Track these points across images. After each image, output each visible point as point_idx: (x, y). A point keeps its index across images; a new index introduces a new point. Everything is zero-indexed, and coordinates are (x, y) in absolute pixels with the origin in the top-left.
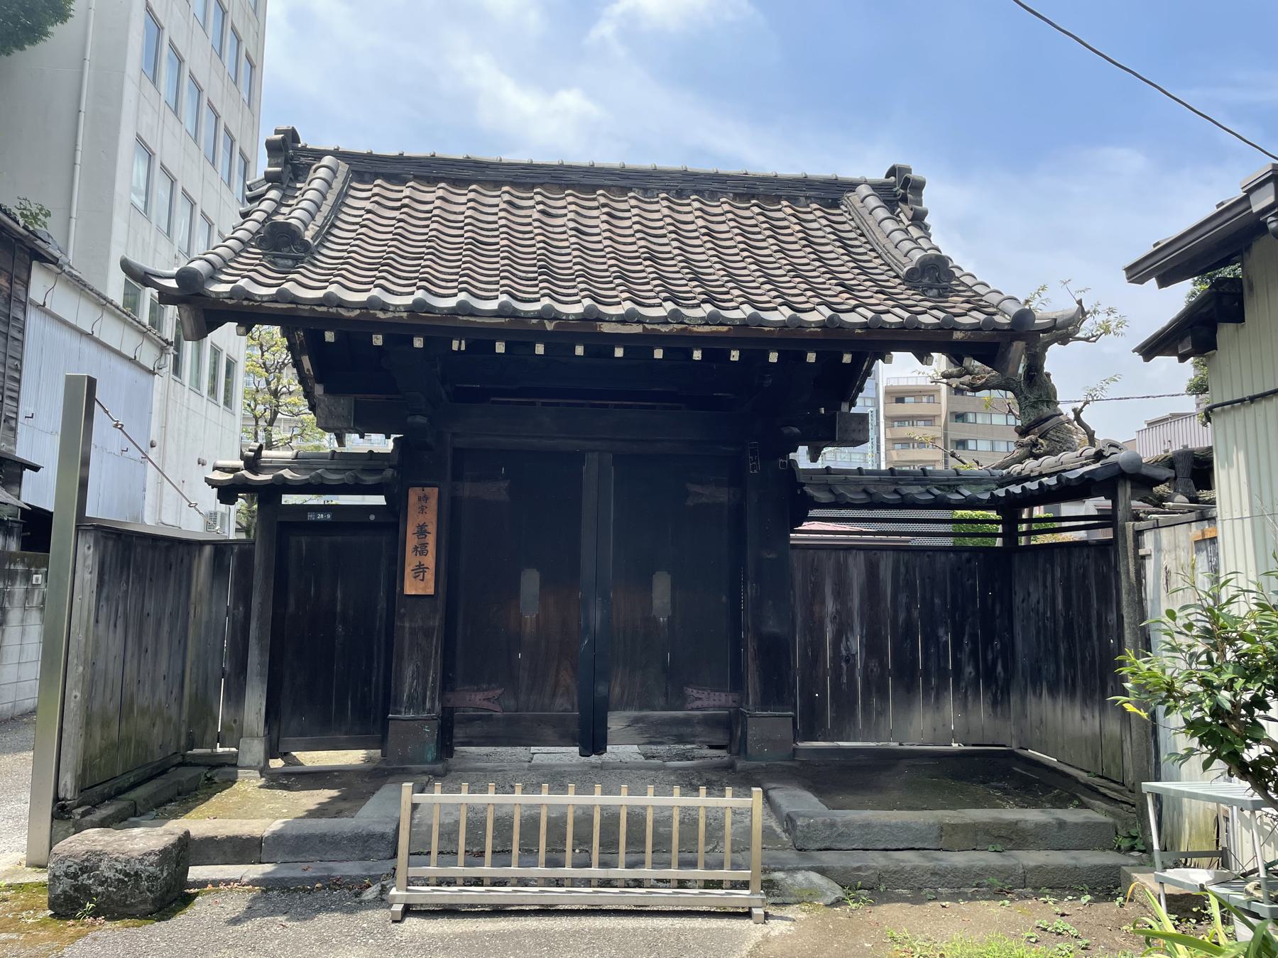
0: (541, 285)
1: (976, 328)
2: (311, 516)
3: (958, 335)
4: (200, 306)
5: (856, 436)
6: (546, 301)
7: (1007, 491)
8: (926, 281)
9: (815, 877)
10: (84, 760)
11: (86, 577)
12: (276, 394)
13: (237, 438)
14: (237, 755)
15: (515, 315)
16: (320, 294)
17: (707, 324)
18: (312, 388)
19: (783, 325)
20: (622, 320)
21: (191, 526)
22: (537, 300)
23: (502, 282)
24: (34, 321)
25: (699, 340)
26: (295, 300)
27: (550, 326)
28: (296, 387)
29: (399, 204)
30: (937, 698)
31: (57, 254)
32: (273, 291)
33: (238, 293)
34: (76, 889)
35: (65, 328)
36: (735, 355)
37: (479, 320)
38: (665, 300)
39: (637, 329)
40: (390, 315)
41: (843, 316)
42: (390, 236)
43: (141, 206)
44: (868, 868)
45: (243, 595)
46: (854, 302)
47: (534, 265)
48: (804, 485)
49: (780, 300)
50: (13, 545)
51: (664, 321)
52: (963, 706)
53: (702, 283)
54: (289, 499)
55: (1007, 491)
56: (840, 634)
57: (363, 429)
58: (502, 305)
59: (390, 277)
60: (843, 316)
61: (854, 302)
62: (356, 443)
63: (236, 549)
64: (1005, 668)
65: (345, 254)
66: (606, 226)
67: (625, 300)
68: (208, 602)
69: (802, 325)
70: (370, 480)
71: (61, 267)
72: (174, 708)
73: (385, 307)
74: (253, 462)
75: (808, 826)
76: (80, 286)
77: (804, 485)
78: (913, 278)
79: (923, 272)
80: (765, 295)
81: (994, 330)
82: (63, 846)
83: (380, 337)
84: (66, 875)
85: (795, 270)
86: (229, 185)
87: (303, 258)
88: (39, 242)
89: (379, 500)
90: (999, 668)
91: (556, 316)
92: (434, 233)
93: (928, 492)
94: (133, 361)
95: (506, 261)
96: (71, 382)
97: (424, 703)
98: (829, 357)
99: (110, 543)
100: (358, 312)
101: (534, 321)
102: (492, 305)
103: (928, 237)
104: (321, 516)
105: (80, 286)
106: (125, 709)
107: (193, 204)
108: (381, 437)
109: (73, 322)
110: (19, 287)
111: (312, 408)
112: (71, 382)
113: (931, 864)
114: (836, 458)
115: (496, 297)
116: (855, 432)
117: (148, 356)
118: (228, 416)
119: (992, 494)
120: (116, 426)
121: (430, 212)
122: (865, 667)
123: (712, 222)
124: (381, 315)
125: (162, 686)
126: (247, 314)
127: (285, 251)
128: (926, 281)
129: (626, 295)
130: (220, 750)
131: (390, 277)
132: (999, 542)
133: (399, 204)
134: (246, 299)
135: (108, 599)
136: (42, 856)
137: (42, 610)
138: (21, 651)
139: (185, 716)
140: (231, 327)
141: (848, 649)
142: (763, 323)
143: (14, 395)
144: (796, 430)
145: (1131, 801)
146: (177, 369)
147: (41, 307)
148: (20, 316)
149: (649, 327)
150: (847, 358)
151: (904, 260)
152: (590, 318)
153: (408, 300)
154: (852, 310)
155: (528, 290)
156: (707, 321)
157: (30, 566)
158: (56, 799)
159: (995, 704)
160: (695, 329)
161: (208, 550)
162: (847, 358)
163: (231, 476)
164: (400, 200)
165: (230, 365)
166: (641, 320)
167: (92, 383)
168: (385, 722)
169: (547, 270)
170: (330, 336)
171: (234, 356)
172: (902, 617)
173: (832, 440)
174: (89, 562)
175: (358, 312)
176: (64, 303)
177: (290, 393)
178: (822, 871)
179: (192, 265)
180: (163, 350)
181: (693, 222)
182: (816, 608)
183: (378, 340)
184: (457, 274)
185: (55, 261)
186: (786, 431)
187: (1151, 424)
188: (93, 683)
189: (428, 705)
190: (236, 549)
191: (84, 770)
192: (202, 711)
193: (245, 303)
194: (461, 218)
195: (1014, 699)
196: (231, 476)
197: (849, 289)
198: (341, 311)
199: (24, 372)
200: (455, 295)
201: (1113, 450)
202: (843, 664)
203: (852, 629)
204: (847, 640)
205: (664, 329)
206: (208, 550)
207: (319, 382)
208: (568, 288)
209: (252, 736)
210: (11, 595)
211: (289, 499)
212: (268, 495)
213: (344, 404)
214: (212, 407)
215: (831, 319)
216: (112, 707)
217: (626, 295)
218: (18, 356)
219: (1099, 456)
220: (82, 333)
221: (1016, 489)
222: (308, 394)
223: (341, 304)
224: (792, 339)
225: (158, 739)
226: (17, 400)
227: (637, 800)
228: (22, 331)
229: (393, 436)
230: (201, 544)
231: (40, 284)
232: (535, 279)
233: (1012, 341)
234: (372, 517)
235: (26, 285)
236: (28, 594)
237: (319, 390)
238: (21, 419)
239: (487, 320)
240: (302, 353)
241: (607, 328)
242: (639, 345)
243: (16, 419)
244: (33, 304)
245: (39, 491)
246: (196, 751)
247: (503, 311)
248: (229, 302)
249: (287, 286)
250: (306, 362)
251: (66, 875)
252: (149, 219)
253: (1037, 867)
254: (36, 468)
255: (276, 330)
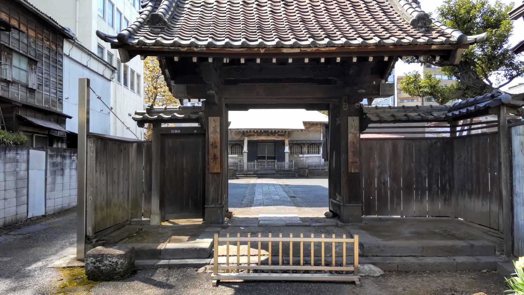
0: (258, 34)
1: (442, 43)
2: (172, 132)
3: (434, 47)
4: (127, 47)
5: (389, 93)
6: (260, 40)
7: (453, 114)
8: (420, 25)
9: (371, 266)
10: (95, 222)
11: (92, 155)
12: (156, 88)
13: (142, 106)
14: (149, 221)
15: (249, 47)
16: (171, 42)
17: (327, 47)
18: (170, 82)
19: (359, 45)
20: (292, 47)
21: (128, 136)
22: (257, 40)
23: (242, 34)
24: (66, 61)
25: (323, 54)
26: (162, 45)
27: (262, 51)
28: (164, 83)
29: (200, 5)
30: (421, 198)
31: (73, 35)
32: (154, 41)
33: (140, 42)
34: (95, 267)
35: (77, 64)
36: (338, 60)
37: (234, 50)
38: (309, 37)
39: (298, 50)
40: (199, 49)
41: (385, 41)
42: (197, 18)
43: (102, 15)
44: (393, 263)
45: (149, 161)
46: (389, 35)
47: (255, 27)
48: (366, 114)
49: (357, 35)
50: (65, 146)
51: (309, 46)
52: (432, 199)
53: (324, 30)
54: (164, 125)
55: (453, 114)
56: (381, 174)
57: (190, 97)
58: (243, 43)
59: (198, 34)
60: (385, 41)
61: (389, 35)
62: (188, 104)
63: (145, 144)
64: (450, 186)
65: (180, 26)
66: (283, 9)
67: (292, 38)
68: (137, 166)
69: (367, 45)
70: (194, 116)
71: (74, 40)
72: (126, 203)
73: (197, 46)
74: (150, 110)
75: (369, 247)
76: (81, 48)
77: (366, 114)
78: (414, 23)
79: (419, 21)
80: (352, 33)
81: (450, 44)
82: (89, 252)
83: (196, 58)
84: (91, 263)
85: (364, 23)
86: (134, 6)
87: (164, 28)
88: (66, 31)
89: (196, 125)
90: (448, 186)
91: (265, 47)
92: (215, 16)
93: (419, 115)
94: (102, 76)
95: (244, 25)
96: (81, 81)
97: (218, 201)
98: (379, 60)
99: (99, 142)
100: (186, 48)
101: (256, 49)
102: (239, 43)
103: (419, 7)
104: (176, 131)
105: (81, 48)
106: (108, 203)
107: (121, 14)
108: (197, 100)
109: (80, 62)
110: (59, 49)
111: (170, 90)
112: (81, 81)
113: (419, 262)
114: (379, 102)
115: (240, 40)
116: (389, 92)
117: (108, 73)
118: (138, 97)
119: (446, 115)
120: (98, 98)
121: (212, 7)
122: (391, 186)
123: (327, 5)
124: (195, 49)
125: (121, 196)
126: (144, 51)
127: (157, 26)
128: (420, 25)
129: (293, 36)
130: (143, 219)
131: (198, 34)
132: (448, 135)
133: (200, 5)
134: (144, 45)
135: (100, 163)
136: (82, 256)
137: (76, 169)
138: (70, 185)
139: (130, 207)
140: (138, 57)
141: (384, 179)
142: (351, 45)
143: (61, 90)
144: (364, 91)
145: (502, 237)
146: (119, 80)
147: (68, 56)
148: (61, 60)
149: (303, 49)
150: (386, 59)
151: (410, 16)
152: (278, 46)
153: (206, 43)
154: (388, 38)
155: (253, 37)
156: (327, 45)
157: (71, 153)
158: (86, 236)
159: (445, 200)
160: (322, 49)
161: (135, 145)
162: (386, 59)
163: (142, 117)
164: (200, 3)
165: (139, 76)
166: (299, 47)
167: (88, 81)
168: (204, 208)
169: (261, 28)
170: (176, 59)
171: (139, 73)
172: (407, 167)
173: (378, 95)
174: (92, 149)
175: (186, 48)
176: (76, 54)
177: (161, 87)
178: (374, 264)
179: (122, 32)
180: (113, 72)
181: (319, 6)
182: (371, 164)
183: (195, 60)
184: (224, 31)
185: (72, 38)
186: (359, 91)
187: (509, 88)
188: (97, 194)
189: (219, 202)
190: (145, 144)
191: (95, 226)
192: (136, 205)
193: (143, 47)
194: (225, 9)
195: (453, 199)
196: (142, 117)
197: (387, 30)
198: (180, 48)
199: (64, 85)
200: (224, 40)
201: (499, 94)
202: (382, 186)
203: (386, 172)
204: (384, 176)
205: (309, 50)
206: (135, 145)
207: (172, 80)
208: (269, 35)
209: (155, 214)
210: (65, 164)
211: (164, 125)
212: (157, 123)
213: (182, 87)
214: (132, 94)
215: (379, 42)
216: (104, 203)
217: (293, 36)
218: (61, 75)
219: (493, 97)
220: (83, 66)
221: (457, 113)
222: (169, 85)
223: (180, 45)
224: (363, 52)
225: (120, 214)
226: (62, 92)
227: (297, 240)
228: (62, 66)
229: (202, 100)
230: (132, 142)
231: (67, 47)
232: (256, 32)
233: (457, 49)
234: (195, 131)
235: (62, 48)
236: (71, 163)
237: (172, 83)
238: (64, 99)
239: (237, 50)
240: (166, 68)
241: (285, 51)
242: (298, 57)
243: (62, 99)
244: (65, 55)
245: (72, 126)
246: (135, 219)
247: (243, 46)
248: (137, 46)
249: (159, 39)
250: (167, 71)
251: (91, 263)
252: (105, 21)
253: (462, 263)
254: (70, 118)
255: (155, 58)
